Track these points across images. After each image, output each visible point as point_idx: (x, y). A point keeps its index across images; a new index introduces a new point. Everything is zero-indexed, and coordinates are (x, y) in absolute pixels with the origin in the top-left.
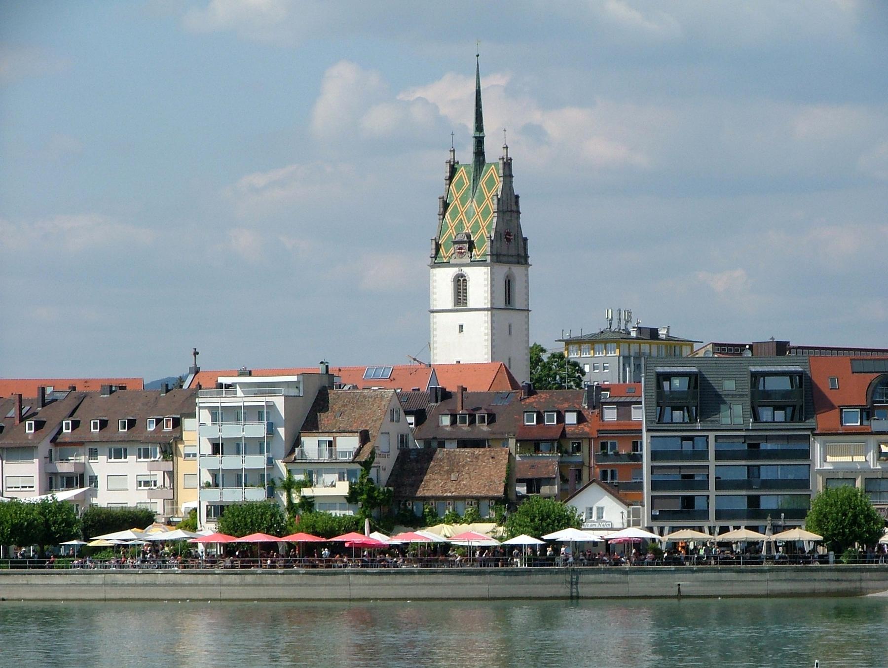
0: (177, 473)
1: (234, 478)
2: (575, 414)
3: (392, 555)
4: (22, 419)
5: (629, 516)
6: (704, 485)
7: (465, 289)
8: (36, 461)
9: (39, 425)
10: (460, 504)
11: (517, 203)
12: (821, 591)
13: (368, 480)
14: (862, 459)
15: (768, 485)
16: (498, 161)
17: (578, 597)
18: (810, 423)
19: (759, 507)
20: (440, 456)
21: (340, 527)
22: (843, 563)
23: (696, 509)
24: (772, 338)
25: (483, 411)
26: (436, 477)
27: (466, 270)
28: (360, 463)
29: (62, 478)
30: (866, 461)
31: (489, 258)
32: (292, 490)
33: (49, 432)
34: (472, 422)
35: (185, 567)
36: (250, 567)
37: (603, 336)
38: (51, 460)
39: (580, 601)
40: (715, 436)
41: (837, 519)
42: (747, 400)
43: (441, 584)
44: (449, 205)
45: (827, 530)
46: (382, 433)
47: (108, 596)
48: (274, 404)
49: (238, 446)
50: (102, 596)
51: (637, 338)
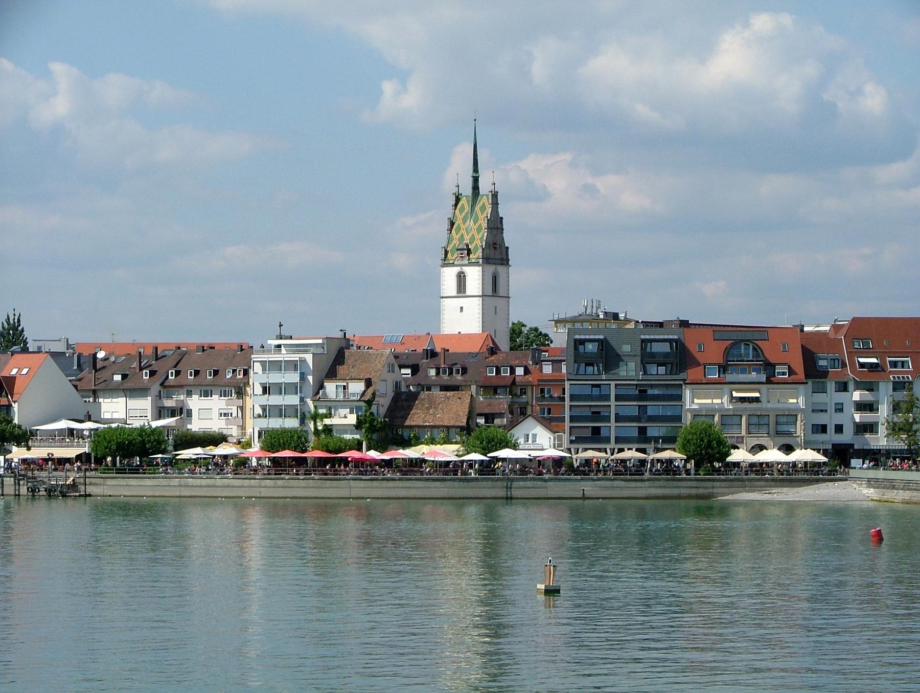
0: (245, 407)
1: (277, 411)
2: (523, 368)
3: (381, 467)
4: (141, 369)
5: (554, 441)
6: (607, 419)
7: (465, 282)
8: (149, 398)
9: (153, 373)
10: (435, 431)
11: (501, 222)
12: (684, 495)
13: (370, 413)
14: (719, 401)
15: (653, 419)
16: (488, 193)
17: (511, 498)
18: (682, 376)
19: (646, 434)
20: (423, 397)
21: (346, 447)
22: (700, 475)
23: (602, 436)
24: (678, 318)
25: (458, 366)
26: (419, 411)
27: (465, 269)
28: (364, 401)
29: (168, 410)
30: (798, 402)
31: (481, 261)
32: (317, 420)
33: (159, 378)
34: (451, 373)
35: (236, 474)
36: (281, 474)
37: (581, 318)
38: (160, 398)
39: (513, 501)
40: (616, 384)
41: (696, 443)
42: (639, 359)
43: (414, 487)
44: (454, 223)
45: (690, 451)
46: (381, 380)
47: (183, 494)
48: (305, 360)
49: (280, 389)
50: (178, 494)
51: (604, 319)
